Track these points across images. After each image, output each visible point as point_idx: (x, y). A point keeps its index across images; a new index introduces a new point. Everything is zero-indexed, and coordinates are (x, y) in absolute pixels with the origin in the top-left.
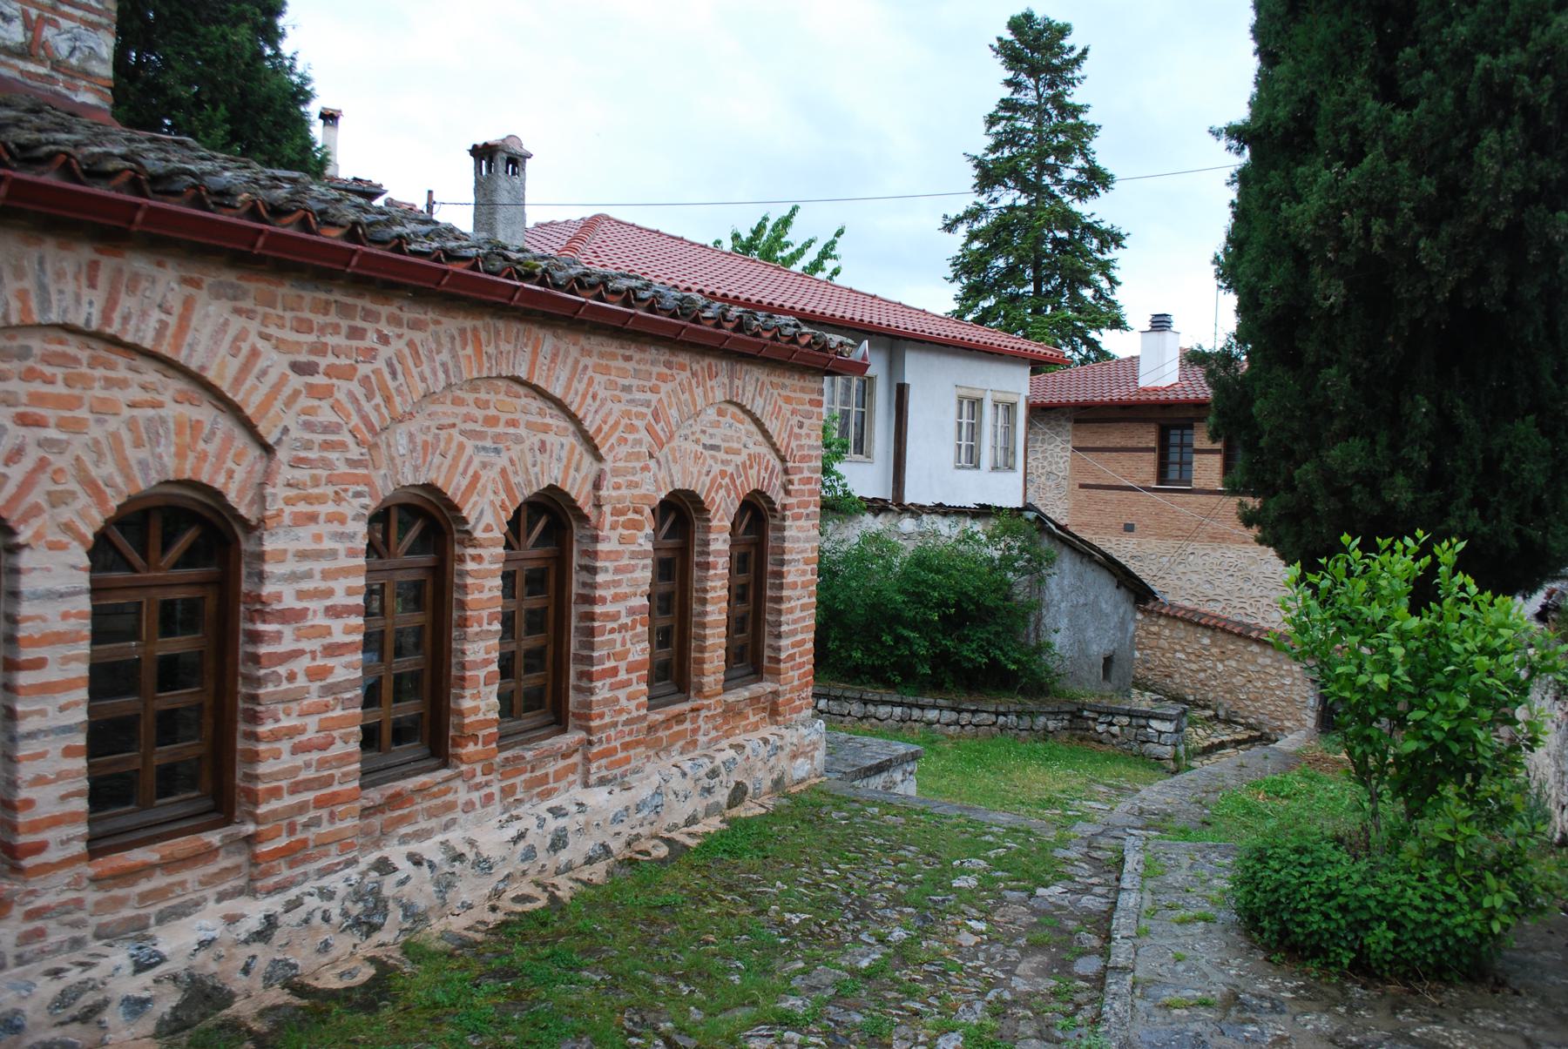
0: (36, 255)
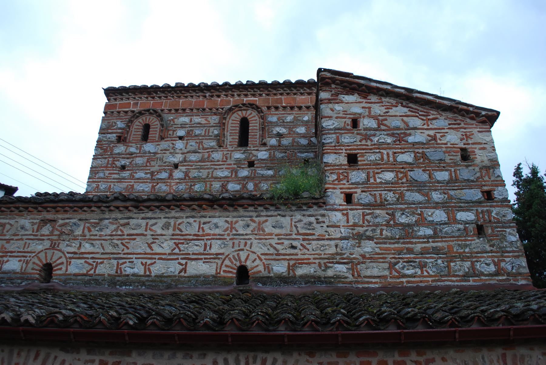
0: (480, 356)
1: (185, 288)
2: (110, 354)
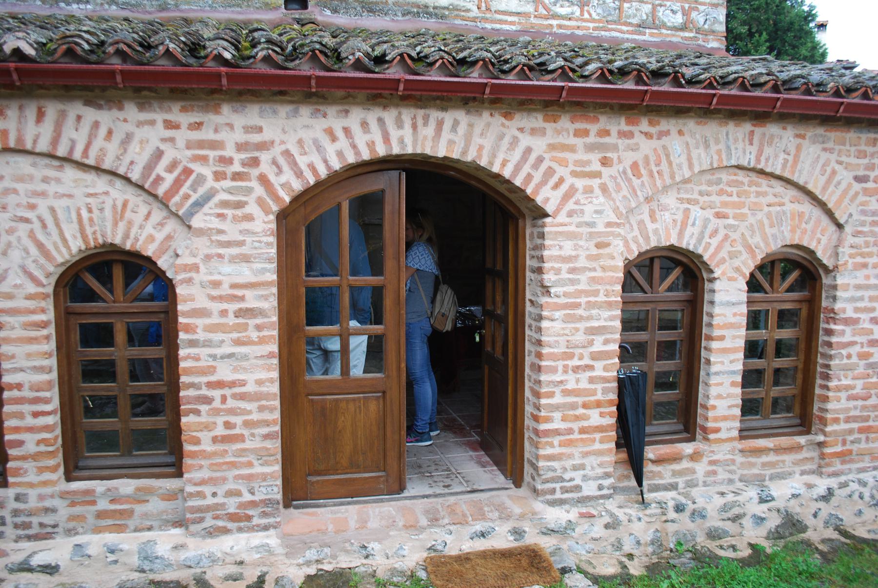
1: (194, 10)
2: (181, 111)
